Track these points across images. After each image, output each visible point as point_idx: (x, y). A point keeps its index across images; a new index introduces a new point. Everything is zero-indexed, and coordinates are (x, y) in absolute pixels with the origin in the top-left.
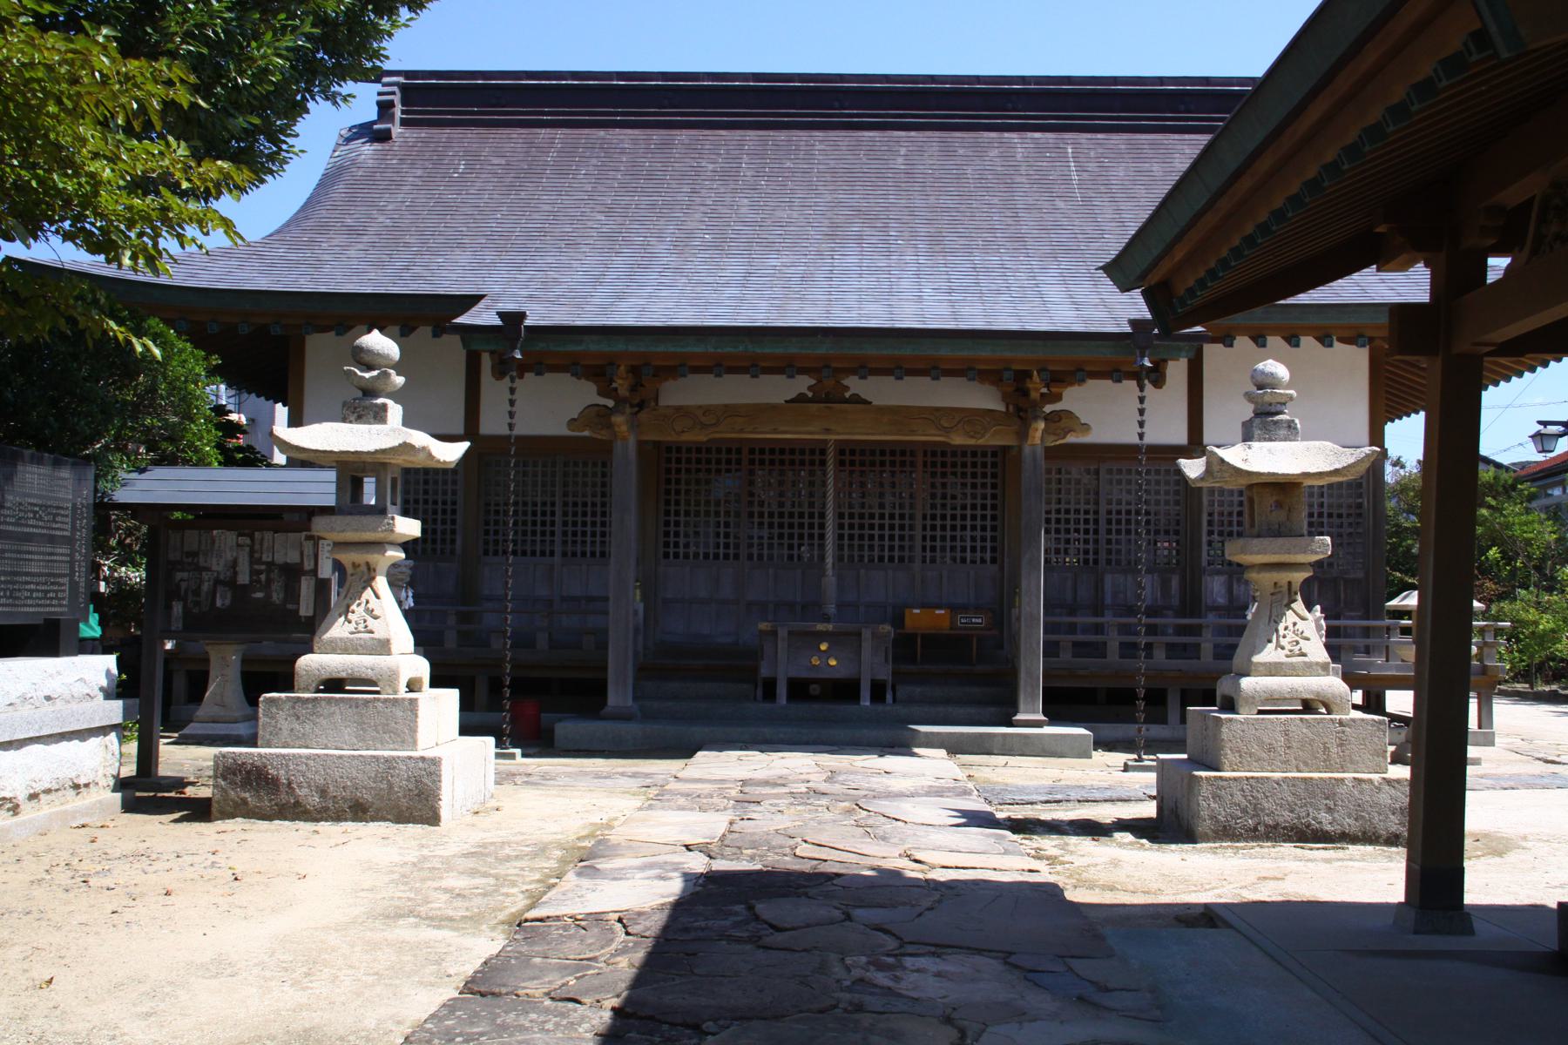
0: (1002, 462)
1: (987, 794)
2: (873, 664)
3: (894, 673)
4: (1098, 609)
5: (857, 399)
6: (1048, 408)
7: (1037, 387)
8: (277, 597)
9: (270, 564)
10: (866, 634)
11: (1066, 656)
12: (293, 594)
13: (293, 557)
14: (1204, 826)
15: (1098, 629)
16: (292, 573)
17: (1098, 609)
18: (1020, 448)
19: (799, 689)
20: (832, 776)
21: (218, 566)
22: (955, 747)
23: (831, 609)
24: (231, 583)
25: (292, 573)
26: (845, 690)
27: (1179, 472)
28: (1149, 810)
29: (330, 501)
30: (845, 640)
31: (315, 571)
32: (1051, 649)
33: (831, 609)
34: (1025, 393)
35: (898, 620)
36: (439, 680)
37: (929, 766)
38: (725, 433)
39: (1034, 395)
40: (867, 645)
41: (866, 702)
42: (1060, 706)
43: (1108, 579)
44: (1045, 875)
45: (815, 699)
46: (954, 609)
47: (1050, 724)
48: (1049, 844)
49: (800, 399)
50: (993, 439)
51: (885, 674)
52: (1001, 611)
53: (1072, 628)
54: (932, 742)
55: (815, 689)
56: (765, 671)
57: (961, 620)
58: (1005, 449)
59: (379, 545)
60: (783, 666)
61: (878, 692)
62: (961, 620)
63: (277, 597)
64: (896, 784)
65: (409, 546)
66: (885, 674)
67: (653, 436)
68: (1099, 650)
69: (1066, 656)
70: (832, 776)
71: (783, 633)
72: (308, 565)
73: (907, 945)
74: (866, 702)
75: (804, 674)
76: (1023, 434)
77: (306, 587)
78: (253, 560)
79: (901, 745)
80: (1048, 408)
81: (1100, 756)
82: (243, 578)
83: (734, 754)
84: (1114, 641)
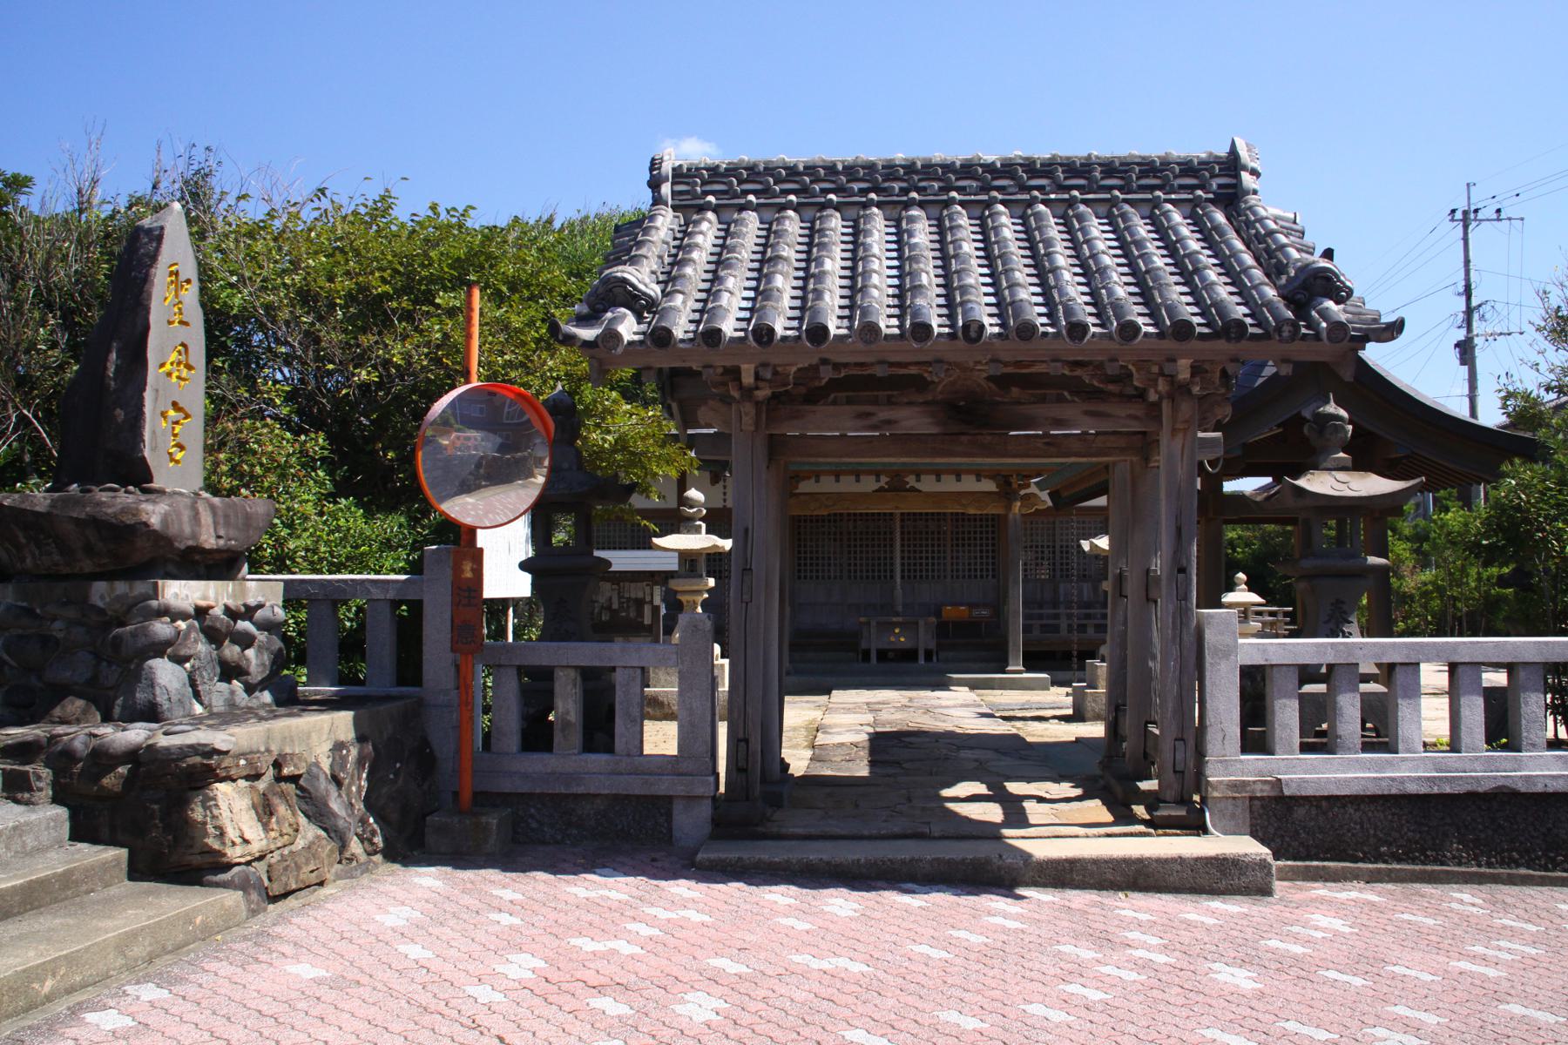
0: (998, 522)
1: (989, 705)
2: (925, 639)
3: (938, 645)
4: (1055, 605)
5: (913, 489)
6: (1022, 492)
7: (1015, 482)
8: (632, 614)
9: (629, 599)
10: (921, 623)
11: (1036, 633)
12: (640, 614)
13: (640, 595)
14: (1088, 715)
15: (1057, 616)
16: (640, 603)
17: (1055, 605)
18: (1006, 516)
19: (883, 655)
20: (911, 700)
21: (602, 600)
22: (973, 686)
23: (900, 609)
24: (609, 608)
25: (640, 603)
26: (909, 655)
27: (1079, 546)
28: (1070, 712)
29: (675, 567)
30: (909, 627)
31: (651, 602)
32: (1027, 629)
33: (900, 609)
34: (1010, 484)
35: (938, 614)
36: (229, 682)
37: (961, 694)
38: (838, 509)
39: (1015, 486)
40: (921, 630)
41: (922, 661)
42: (1033, 662)
43: (1062, 586)
44: (1014, 731)
45: (892, 660)
46: (971, 606)
47: (1028, 671)
48: (1019, 724)
49: (881, 490)
50: (993, 509)
51: (932, 645)
52: (998, 606)
53: (1041, 617)
54: (960, 683)
55: (891, 655)
56: (864, 645)
57: (975, 613)
58: (995, 518)
59: (700, 592)
60: (874, 641)
61: (929, 655)
62: (975, 613)
63: (632, 614)
64: (944, 703)
65: (710, 591)
66: (932, 645)
67: (796, 512)
68: (1056, 629)
69: (1036, 633)
70: (911, 700)
71: (873, 623)
72: (648, 599)
73: (959, 748)
74: (922, 661)
75: (887, 647)
76: (1009, 508)
77: (647, 610)
78: (620, 597)
79: (943, 685)
80: (1022, 492)
81: (1054, 689)
82: (615, 606)
83: (854, 692)
84: (1064, 624)
